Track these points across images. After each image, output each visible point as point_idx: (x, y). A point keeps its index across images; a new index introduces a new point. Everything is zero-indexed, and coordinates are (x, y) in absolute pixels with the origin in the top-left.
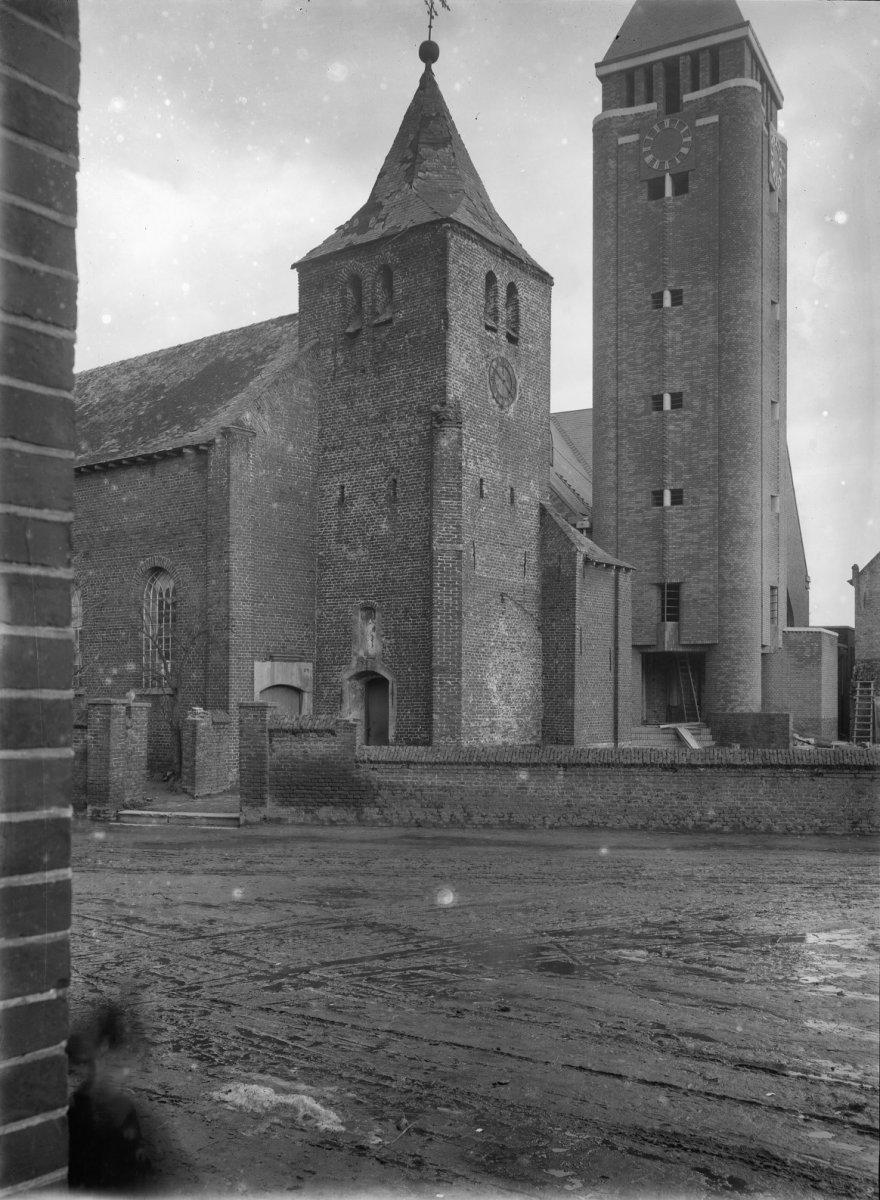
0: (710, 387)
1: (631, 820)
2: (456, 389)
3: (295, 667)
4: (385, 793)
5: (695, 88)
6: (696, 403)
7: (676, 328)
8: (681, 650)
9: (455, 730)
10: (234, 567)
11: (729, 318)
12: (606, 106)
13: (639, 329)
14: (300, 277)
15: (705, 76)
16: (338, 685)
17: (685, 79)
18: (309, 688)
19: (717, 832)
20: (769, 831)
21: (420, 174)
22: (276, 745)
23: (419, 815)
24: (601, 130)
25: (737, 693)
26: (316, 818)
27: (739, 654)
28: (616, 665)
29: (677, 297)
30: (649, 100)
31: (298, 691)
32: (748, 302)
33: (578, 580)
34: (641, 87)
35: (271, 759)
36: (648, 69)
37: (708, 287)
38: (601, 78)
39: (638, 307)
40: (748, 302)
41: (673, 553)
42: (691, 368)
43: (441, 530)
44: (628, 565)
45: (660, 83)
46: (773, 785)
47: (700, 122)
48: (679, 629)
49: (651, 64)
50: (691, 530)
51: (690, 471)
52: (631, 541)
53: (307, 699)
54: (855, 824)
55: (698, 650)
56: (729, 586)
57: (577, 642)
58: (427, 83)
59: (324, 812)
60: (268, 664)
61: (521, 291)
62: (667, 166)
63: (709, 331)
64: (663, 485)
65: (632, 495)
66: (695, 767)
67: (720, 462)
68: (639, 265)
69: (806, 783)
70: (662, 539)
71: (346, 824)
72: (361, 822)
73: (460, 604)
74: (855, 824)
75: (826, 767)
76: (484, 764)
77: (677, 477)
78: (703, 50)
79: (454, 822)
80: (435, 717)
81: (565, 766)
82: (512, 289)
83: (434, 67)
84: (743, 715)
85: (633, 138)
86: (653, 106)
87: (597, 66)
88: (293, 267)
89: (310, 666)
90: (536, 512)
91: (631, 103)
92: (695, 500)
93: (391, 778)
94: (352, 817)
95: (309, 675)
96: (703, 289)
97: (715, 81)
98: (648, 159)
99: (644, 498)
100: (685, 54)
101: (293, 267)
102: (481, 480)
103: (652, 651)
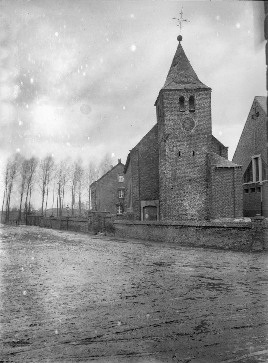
3: (153, 201)
58: (180, 47)
59: (111, 233)
60: (145, 201)
75: (169, 225)
82: (192, 100)
83: (181, 42)
90: (205, 156)
102: (180, 152)
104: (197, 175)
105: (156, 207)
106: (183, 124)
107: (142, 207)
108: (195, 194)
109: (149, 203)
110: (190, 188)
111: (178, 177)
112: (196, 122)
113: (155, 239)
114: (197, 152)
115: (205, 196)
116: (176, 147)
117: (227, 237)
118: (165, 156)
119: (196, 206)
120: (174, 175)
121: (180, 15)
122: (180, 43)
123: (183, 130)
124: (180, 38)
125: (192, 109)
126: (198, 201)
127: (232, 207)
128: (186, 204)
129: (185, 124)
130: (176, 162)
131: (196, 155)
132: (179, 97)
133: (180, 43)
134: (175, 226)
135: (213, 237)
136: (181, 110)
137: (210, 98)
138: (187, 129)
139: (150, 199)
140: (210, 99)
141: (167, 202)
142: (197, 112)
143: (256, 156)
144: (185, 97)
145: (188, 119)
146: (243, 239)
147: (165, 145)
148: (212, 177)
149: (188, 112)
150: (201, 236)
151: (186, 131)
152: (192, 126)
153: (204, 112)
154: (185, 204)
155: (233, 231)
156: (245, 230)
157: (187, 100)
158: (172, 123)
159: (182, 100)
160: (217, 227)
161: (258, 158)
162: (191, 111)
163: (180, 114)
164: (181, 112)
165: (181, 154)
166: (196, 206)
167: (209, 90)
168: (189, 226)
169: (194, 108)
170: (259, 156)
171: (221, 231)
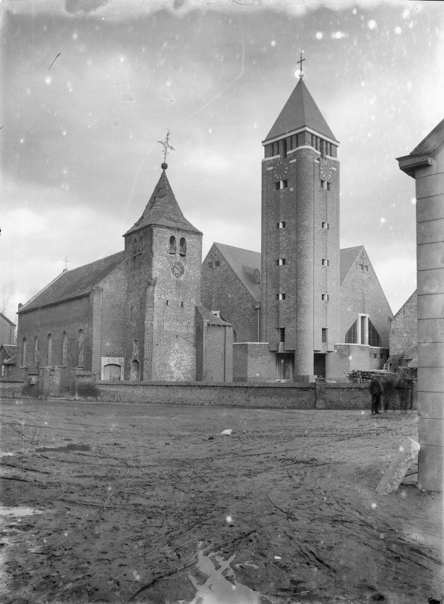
0: (293, 257)
1: (158, 401)
2: (156, 274)
3: (117, 359)
4: (102, 393)
5: (291, 149)
6: (289, 262)
7: (283, 236)
8: (285, 352)
9: (150, 377)
10: (94, 329)
11: (299, 232)
12: (266, 156)
13: (273, 236)
14: (125, 239)
15: (294, 145)
16: (129, 364)
17: (288, 147)
18: (123, 365)
19: (178, 404)
20: (190, 404)
21: (154, 207)
22: (78, 380)
23: (110, 399)
24: (264, 164)
25: (301, 368)
26: (87, 399)
27: (302, 354)
28: (225, 357)
29: (284, 224)
30: (278, 154)
31: (120, 366)
32: (305, 226)
33: (204, 330)
34: (276, 149)
35: (77, 384)
36: (278, 142)
37: (293, 221)
38: (265, 146)
39: (273, 228)
40: (305, 226)
41: (282, 317)
42: (288, 250)
43: (148, 317)
44: (230, 324)
45: (282, 147)
46: (191, 391)
47: (291, 162)
48: (284, 344)
49: (279, 140)
50: (287, 309)
51: (287, 287)
52: (270, 312)
53: (122, 369)
54: (210, 403)
55: (288, 352)
56: (299, 329)
57: (204, 350)
58: (163, 178)
59: (89, 398)
60: (107, 358)
61: (187, 240)
62: (281, 178)
63: (293, 236)
64: (279, 292)
65: (271, 296)
66: (172, 386)
67: (297, 284)
68: (273, 213)
69: (198, 391)
70: (278, 312)
71: (94, 401)
72: (97, 401)
73: (152, 340)
74: (210, 403)
75: (203, 386)
76: (125, 385)
77: (283, 289)
78: (293, 135)
79: (117, 401)
80: (144, 374)
81: (143, 386)
82: (183, 241)
83: (166, 170)
84: (303, 376)
85: (271, 168)
86: (279, 156)
87: (263, 142)
88: (123, 236)
89: (123, 358)
90: (193, 309)
91: (273, 155)
92: (289, 297)
93: (103, 389)
94: (94, 399)
95: (123, 361)
96: (292, 221)
97: (297, 146)
98: (276, 175)
99: (274, 297)
100: (288, 137)
101: (123, 236)
102: (168, 301)
103: (319, 353)
104: (184, 331)
105: (120, 366)
106: (173, 269)
107: (103, 364)
108: (182, 353)
109: (112, 360)
110: (177, 346)
111: (164, 330)
112: (186, 268)
113: (178, 402)
114: (186, 304)
115: (192, 356)
116: (164, 294)
117: (286, 397)
118: (153, 304)
119: (182, 368)
120: (161, 327)
121: (166, 140)
122: (164, 171)
123: (172, 276)
124: (164, 166)
125: (182, 253)
126: (185, 362)
127: (223, 371)
128: (172, 364)
129: (175, 269)
130: (163, 312)
131: (184, 306)
132: (170, 236)
133: (164, 171)
134: (213, 386)
135: (268, 397)
136: (171, 252)
137: (201, 243)
138: (177, 275)
139: (113, 355)
140: (201, 245)
141: (153, 360)
142: (187, 257)
143: (363, 315)
144: (176, 237)
145: (178, 263)
146: (305, 398)
147: (154, 291)
148: (204, 335)
149: (178, 255)
150: (252, 397)
151: (175, 278)
152: (182, 272)
153: (195, 258)
154: (170, 364)
155: (294, 391)
156: (307, 390)
157: (178, 241)
158: (161, 265)
159: (172, 239)
160: (275, 388)
161: (365, 317)
162: (181, 255)
163: (170, 257)
164: (171, 253)
165: (169, 304)
166: (182, 368)
167: (199, 234)
168: (235, 387)
169: (185, 252)
170: (367, 316)
171: (278, 391)
